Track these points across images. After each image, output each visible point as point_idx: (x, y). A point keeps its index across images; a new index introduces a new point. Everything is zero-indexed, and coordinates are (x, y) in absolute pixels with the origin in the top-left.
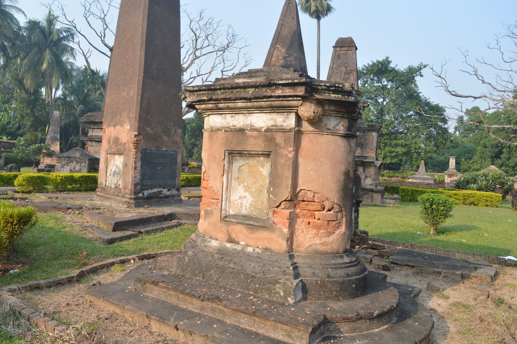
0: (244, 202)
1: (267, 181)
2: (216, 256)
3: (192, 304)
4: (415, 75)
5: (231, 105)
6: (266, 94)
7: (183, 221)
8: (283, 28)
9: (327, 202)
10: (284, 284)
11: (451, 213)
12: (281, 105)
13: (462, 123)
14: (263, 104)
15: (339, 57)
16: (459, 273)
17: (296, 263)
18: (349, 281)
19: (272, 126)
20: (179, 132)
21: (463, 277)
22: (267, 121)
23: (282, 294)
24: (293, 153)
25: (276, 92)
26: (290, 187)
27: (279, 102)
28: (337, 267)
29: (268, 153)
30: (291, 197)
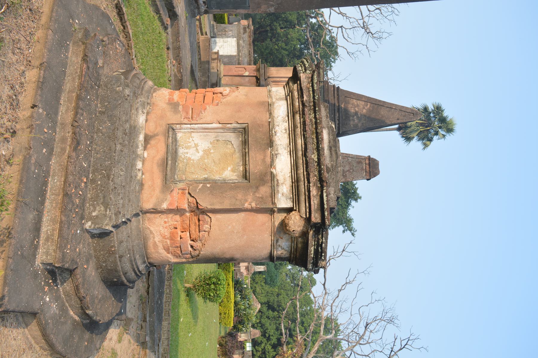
0: (192, 151)
1: (217, 177)
2: (127, 126)
3: (67, 111)
4: (344, 225)
5: (298, 130)
6: (311, 175)
7: (169, 30)
8: (388, 109)
9: (201, 245)
10: (105, 215)
11: (208, 301)
14: (301, 171)
15: (359, 163)
16: (148, 339)
17: (130, 221)
18: (120, 276)
19: (277, 180)
20: (270, 9)
21: (143, 344)
22: (283, 174)
24: (249, 207)
25: (314, 188)
26: (212, 207)
27: (303, 190)
28: (132, 261)
29: (248, 178)
30: (202, 209)
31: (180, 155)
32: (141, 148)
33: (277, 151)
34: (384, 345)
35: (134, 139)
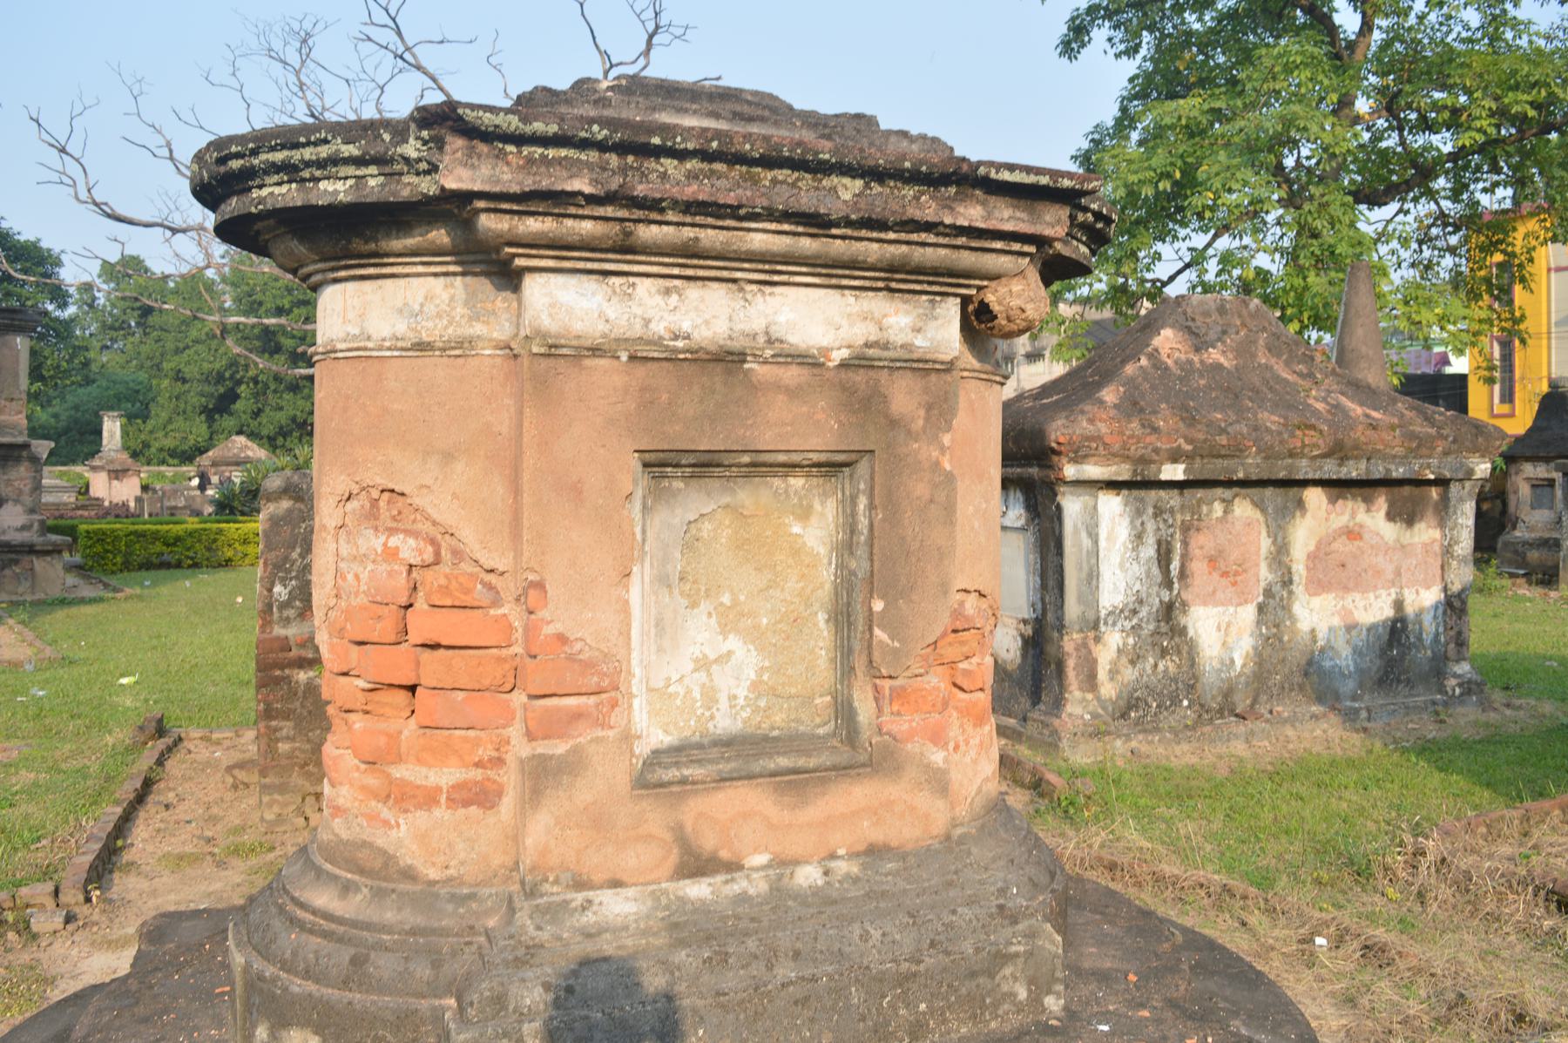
0: (724, 680)
1: (826, 575)
5: (710, 237)
6: (914, 213)
10: (1030, 954)
12: (948, 263)
13: (91, 306)
19: (867, 345)
22: (844, 323)
23: (1023, 994)
25: (961, 210)
27: (943, 252)
29: (853, 456)
31: (740, 725)
32: (740, 885)
33: (755, 336)
34: (363, 76)
35: (724, 918)
